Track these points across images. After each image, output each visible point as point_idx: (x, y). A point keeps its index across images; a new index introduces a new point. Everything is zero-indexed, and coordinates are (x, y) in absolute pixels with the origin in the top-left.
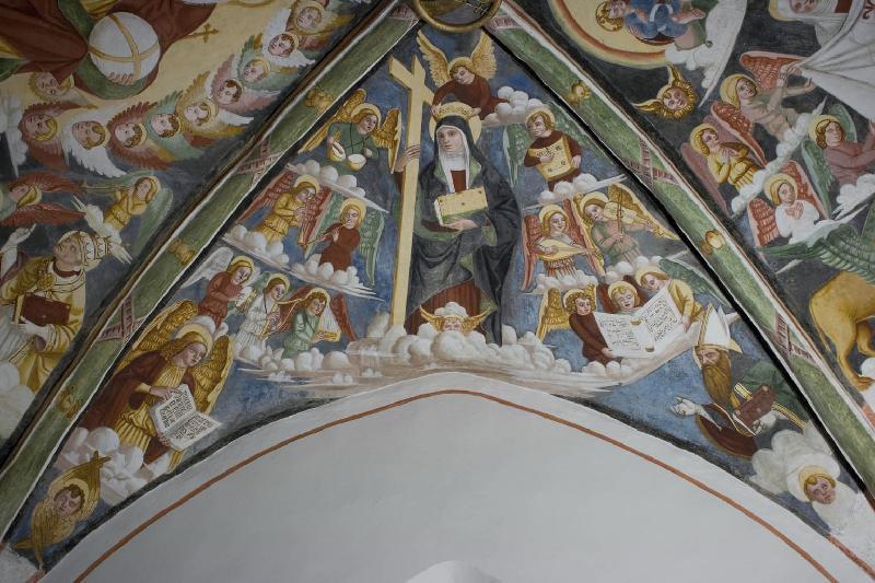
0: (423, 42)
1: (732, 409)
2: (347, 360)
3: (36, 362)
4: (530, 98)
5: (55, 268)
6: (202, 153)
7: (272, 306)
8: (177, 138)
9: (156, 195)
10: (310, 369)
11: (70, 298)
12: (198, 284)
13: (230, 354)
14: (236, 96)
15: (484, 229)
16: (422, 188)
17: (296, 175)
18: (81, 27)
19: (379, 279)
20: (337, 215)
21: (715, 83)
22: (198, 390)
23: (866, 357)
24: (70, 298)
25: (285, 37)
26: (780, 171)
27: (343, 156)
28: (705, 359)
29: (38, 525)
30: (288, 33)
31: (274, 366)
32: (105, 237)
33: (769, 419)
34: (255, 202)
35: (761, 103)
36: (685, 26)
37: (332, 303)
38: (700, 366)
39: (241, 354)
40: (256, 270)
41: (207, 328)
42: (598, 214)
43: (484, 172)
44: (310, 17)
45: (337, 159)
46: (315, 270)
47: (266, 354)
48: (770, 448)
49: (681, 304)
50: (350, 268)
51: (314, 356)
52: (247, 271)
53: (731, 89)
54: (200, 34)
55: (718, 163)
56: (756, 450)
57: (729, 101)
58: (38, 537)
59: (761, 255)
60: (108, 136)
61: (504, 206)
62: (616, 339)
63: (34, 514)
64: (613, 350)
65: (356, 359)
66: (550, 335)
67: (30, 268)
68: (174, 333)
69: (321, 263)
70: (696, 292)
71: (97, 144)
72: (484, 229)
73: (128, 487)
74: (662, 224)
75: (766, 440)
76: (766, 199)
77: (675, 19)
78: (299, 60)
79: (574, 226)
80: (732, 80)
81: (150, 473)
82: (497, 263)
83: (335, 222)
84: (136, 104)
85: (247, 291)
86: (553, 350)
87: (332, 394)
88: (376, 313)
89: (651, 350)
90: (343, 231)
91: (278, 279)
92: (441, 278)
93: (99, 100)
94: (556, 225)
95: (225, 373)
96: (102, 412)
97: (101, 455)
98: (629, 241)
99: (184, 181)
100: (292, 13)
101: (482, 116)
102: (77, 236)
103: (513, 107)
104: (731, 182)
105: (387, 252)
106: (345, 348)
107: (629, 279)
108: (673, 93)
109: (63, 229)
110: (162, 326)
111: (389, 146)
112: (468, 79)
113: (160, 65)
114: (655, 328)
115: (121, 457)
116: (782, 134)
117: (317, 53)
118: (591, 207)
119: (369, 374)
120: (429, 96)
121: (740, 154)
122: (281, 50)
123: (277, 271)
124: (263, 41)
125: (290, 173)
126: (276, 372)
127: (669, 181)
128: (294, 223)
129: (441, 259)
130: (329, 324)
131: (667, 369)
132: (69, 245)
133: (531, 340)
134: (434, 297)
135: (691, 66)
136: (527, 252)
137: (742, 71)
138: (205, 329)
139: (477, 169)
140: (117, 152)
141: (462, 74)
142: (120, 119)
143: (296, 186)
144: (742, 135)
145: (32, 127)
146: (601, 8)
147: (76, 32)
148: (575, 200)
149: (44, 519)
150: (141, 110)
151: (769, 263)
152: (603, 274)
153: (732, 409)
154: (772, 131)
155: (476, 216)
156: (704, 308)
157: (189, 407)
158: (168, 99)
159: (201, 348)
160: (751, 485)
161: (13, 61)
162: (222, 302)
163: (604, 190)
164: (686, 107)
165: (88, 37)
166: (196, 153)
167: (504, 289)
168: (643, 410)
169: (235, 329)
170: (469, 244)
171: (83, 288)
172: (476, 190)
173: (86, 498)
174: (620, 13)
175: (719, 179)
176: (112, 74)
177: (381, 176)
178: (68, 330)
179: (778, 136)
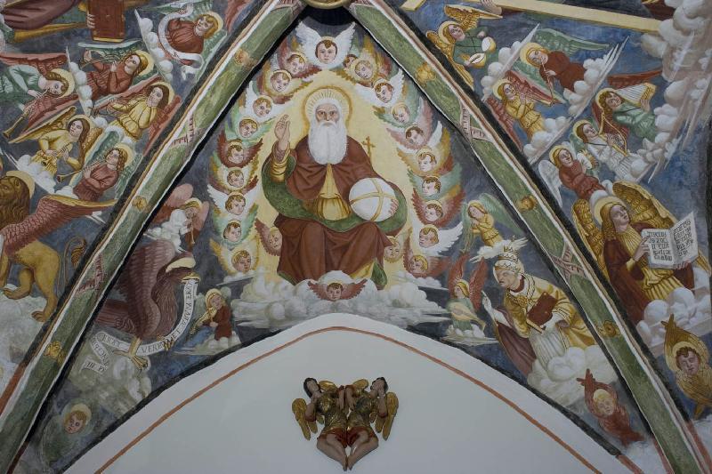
3: (575, 332)
7: (601, 140)
8: (444, 181)
9: (481, 207)
11: (539, 290)
12: (563, 194)
13: (632, 186)
14: (419, 131)
18: (357, 222)
19: (604, 39)
20: (533, 68)
23: (333, 166)
24: (539, 290)
25: (378, 88)
27: (482, 55)
29: (693, 392)
31: (659, 151)
32: (503, 250)
34: (508, 133)
39: (635, 176)
40: (565, 145)
41: (601, 198)
45: (484, 60)
46: (578, 96)
47: (644, 156)
50: (584, 66)
51: (663, 113)
52: (563, 152)
54: (369, 149)
58: (701, 397)
60: (433, 226)
61: (273, 292)
63: (682, 390)
67: (510, 307)
68: (597, 224)
69: (572, 89)
78: (398, 80)
81: (703, 289)
84: (412, 202)
85: (580, 157)
88: (639, 47)
90: (548, 66)
91: (578, 128)
95: (647, 194)
96: (631, 302)
99: (477, 183)
105: (577, 28)
109: (490, 275)
110: (587, 231)
111: (476, 17)
113: (387, 180)
115: (676, 305)
122: (388, 93)
124: (379, 106)
125: (489, 100)
132: (501, 277)
138: (602, 199)
140: (444, 223)
142: (421, 215)
143: (500, 98)
145: (418, 270)
147: (359, 227)
150: (417, 199)
157: (663, 235)
161: (375, 266)
162: (584, 179)
165: (363, 220)
166: (458, 168)
169: (611, 175)
171: (535, 279)
177: (503, 27)
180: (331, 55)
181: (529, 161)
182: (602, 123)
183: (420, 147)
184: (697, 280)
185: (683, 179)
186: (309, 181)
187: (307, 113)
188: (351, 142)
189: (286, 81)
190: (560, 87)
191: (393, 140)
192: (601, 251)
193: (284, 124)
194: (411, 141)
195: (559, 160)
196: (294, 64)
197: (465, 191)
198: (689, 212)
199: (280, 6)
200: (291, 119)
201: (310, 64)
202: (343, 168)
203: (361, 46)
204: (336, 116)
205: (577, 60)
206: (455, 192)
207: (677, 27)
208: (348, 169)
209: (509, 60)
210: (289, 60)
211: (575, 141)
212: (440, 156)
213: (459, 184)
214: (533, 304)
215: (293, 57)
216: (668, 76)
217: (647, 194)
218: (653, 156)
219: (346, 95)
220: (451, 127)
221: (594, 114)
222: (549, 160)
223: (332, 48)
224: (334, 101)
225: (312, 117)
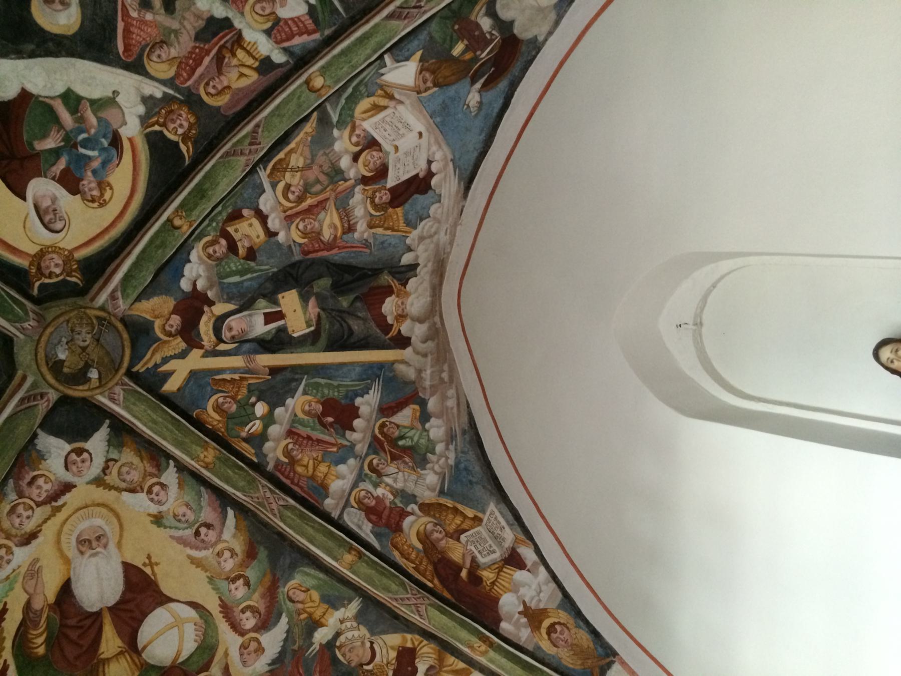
0: (143, 367)
1: (476, 59)
2: (435, 397)
4: (189, 261)
5: (368, 664)
6: (262, 549)
7: (392, 469)
10: (443, 429)
11: (392, 648)
12: (377, 535)
13: (434, 501)
14: (208, 526)
15: (316, 290)
16: (283, 349)
17: (278, 463)
19: (364, 377)
20: (311, 420)
21: (156, 84)
22: (465, 526)
24: (392, 648)
25: (150, 492)
26: (242, 14)
27: (258, 422)
28: (429, 84)
30: (145, 490)
33: (486, 23)
34: (303, 494)
35: (173, 35)
36: (99, 120)
37: (388, 417)
38: (436, 89)
39: (433, 490)
40: (362, 485)
42: (297, 190)
43: (264, 296)
44: (128, 473)
45: (261, 427)
47: (433, 469)
48: (512, 23)
49: (377, 109)
50: (356, 404)
51: (432, 427)
52: (363, 493)
53: (161, 68)
55: (238, 78)
56: (514, 35)
57: (174, 68)
58: (590, 661)
59: (327, 32)
62: (412, 166)
63: (571, 666)
64: (420, 168)
65: (434, 389)
66: (408, 223)
68: (418, 551)
69: (353, 430)
70: (366, 94)
71: (259, 643)
72: (316, 290)
73: (546, 583)
74: (302, 130)
75: (505, 27)
76: (272, 28)
77: (93, 131)
78: (170, 476)
79: (309, 210)
80: (151, 68)
81: (534, 564)
82: (346, 275)
83: (316, 421)
85: (380, 491)
86: (421, 220)
87: (463, 407)
89: (420, 134)
90: (325, 414)
92: (361, 322)
93: (220, 646)
94: (309, 227)
95: (449, 503)
97: (521, 608)
98: (321, 159)
99: (288, 561)
100: (126, 490)
101: (211, 303)
102: (339, 648)
103: (200, 276)
104: (257, 64)
105: (340, 372)
106: (424, 399)
107: (356, 158)
108: (171, 126)
109: (335, 660)
110: (413, 562)
111: (246, 383)
112: (176, 320)
114: (401, 132)
115: (522, 591)
116: (203, 12)
117: (163, 460)
118: (291, 196)
119: (445, 375)
120: (196, 353)
121: (228, 55)
122: (162, 493)
123: (362, 468)
125: (276, 467)
126: (447, 458)
127: (260, 130)
128: (320, 459)
129: (344, 325)
130: (405, 417)
131: (438, 119)
132: (348, 655)
133: (413, 240)
134: (378, 326)
135: (141, 110)
136: (335, 251)
137: (140, 56)
139: (262, 303)
140: (265, 625)
141: (172, 326)
142: (235, 627)
143: (286, 460)
144: (208, 53)
146: (90, 204)
148: (285, 212)
149: (575, 657)
150: (226, 610)
151: (335, 24)
152: (352, 181)
153: (476, 59)
154: (201, 23)
155: (304, 299)
156: (381, 87)
158: (216, 589)
159: (430, 527)
160: (546, 40)
163: (274, 186)
164: (184, 112)
165: (164, 667)
166: (263, 554)
167: (370, 267)
168: (475, 140)
170: (331, 301)
171: (383, 637)
172: (282, 301)
173: (556, 620)
174: (93, 185)
175: (254, 76)
176: (196, 641)
178: (419, 648)
179: (206, 16)
180: (84, 465)
181: (333, 516)
182: (388, 453)
183: (216, 543)
184: (525, 558)
185: (470, 478)
186: (81, 642)
187: (64, 546)
188: (129, 569)
189: (30, 512)
190: (341, 431)
191: (180, 547)
192: (433, 576)
193: (34, 572)
194: (203, 541)
195: (362, 503)
196: (39, 487)
197: (278, 574)
198: (489, 504)
199: (19, 409)
200: (43, 563)
201: (60, 482)
202: (122, 607)
203: (120, 446)
204: (103, 541)
205: (348, 401)
206: (268, 579)
207: (417, 353)
208: (131, 606)
209: (286, 420)
210: (31, 483)
211: (370, 478)
212: (239, 547)
213: (269, 570)
214: (393, 667)
215: (34, 478)
216: (425, 395)
217: (449, 503)
218: (440, 466)
219: (112, 510)
220: (241, 509)
221: (378, 447)
222: (353, 507)
223: (85, 455)
224: (99, 521)
225: (71, 550)
